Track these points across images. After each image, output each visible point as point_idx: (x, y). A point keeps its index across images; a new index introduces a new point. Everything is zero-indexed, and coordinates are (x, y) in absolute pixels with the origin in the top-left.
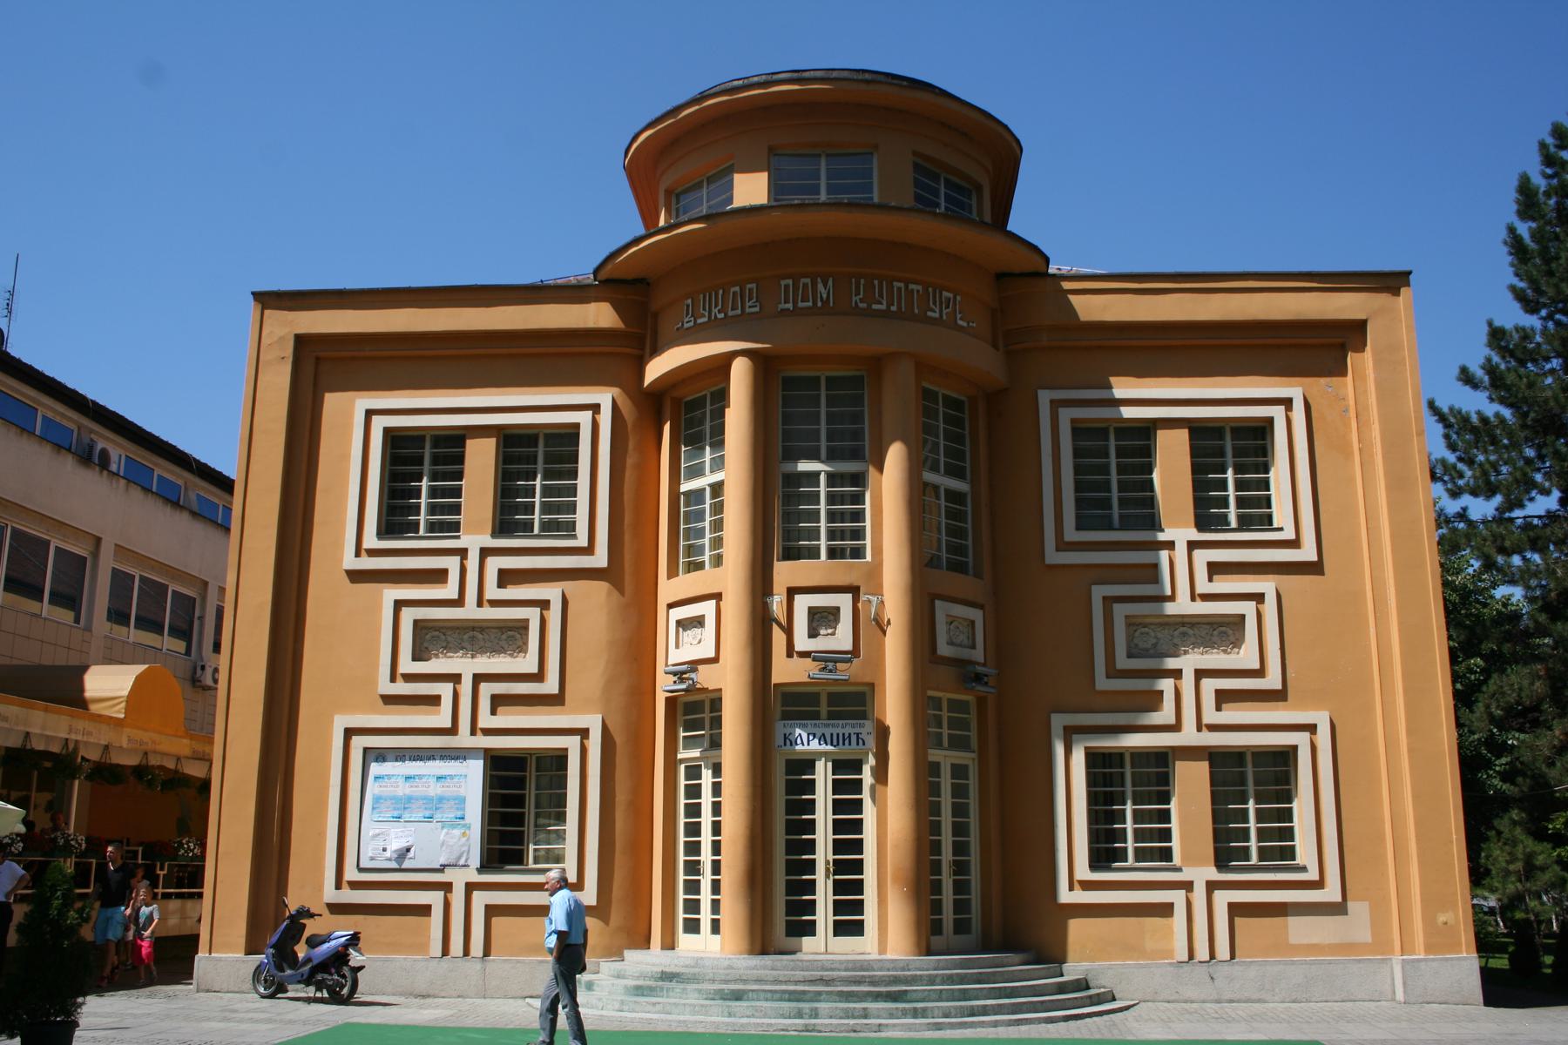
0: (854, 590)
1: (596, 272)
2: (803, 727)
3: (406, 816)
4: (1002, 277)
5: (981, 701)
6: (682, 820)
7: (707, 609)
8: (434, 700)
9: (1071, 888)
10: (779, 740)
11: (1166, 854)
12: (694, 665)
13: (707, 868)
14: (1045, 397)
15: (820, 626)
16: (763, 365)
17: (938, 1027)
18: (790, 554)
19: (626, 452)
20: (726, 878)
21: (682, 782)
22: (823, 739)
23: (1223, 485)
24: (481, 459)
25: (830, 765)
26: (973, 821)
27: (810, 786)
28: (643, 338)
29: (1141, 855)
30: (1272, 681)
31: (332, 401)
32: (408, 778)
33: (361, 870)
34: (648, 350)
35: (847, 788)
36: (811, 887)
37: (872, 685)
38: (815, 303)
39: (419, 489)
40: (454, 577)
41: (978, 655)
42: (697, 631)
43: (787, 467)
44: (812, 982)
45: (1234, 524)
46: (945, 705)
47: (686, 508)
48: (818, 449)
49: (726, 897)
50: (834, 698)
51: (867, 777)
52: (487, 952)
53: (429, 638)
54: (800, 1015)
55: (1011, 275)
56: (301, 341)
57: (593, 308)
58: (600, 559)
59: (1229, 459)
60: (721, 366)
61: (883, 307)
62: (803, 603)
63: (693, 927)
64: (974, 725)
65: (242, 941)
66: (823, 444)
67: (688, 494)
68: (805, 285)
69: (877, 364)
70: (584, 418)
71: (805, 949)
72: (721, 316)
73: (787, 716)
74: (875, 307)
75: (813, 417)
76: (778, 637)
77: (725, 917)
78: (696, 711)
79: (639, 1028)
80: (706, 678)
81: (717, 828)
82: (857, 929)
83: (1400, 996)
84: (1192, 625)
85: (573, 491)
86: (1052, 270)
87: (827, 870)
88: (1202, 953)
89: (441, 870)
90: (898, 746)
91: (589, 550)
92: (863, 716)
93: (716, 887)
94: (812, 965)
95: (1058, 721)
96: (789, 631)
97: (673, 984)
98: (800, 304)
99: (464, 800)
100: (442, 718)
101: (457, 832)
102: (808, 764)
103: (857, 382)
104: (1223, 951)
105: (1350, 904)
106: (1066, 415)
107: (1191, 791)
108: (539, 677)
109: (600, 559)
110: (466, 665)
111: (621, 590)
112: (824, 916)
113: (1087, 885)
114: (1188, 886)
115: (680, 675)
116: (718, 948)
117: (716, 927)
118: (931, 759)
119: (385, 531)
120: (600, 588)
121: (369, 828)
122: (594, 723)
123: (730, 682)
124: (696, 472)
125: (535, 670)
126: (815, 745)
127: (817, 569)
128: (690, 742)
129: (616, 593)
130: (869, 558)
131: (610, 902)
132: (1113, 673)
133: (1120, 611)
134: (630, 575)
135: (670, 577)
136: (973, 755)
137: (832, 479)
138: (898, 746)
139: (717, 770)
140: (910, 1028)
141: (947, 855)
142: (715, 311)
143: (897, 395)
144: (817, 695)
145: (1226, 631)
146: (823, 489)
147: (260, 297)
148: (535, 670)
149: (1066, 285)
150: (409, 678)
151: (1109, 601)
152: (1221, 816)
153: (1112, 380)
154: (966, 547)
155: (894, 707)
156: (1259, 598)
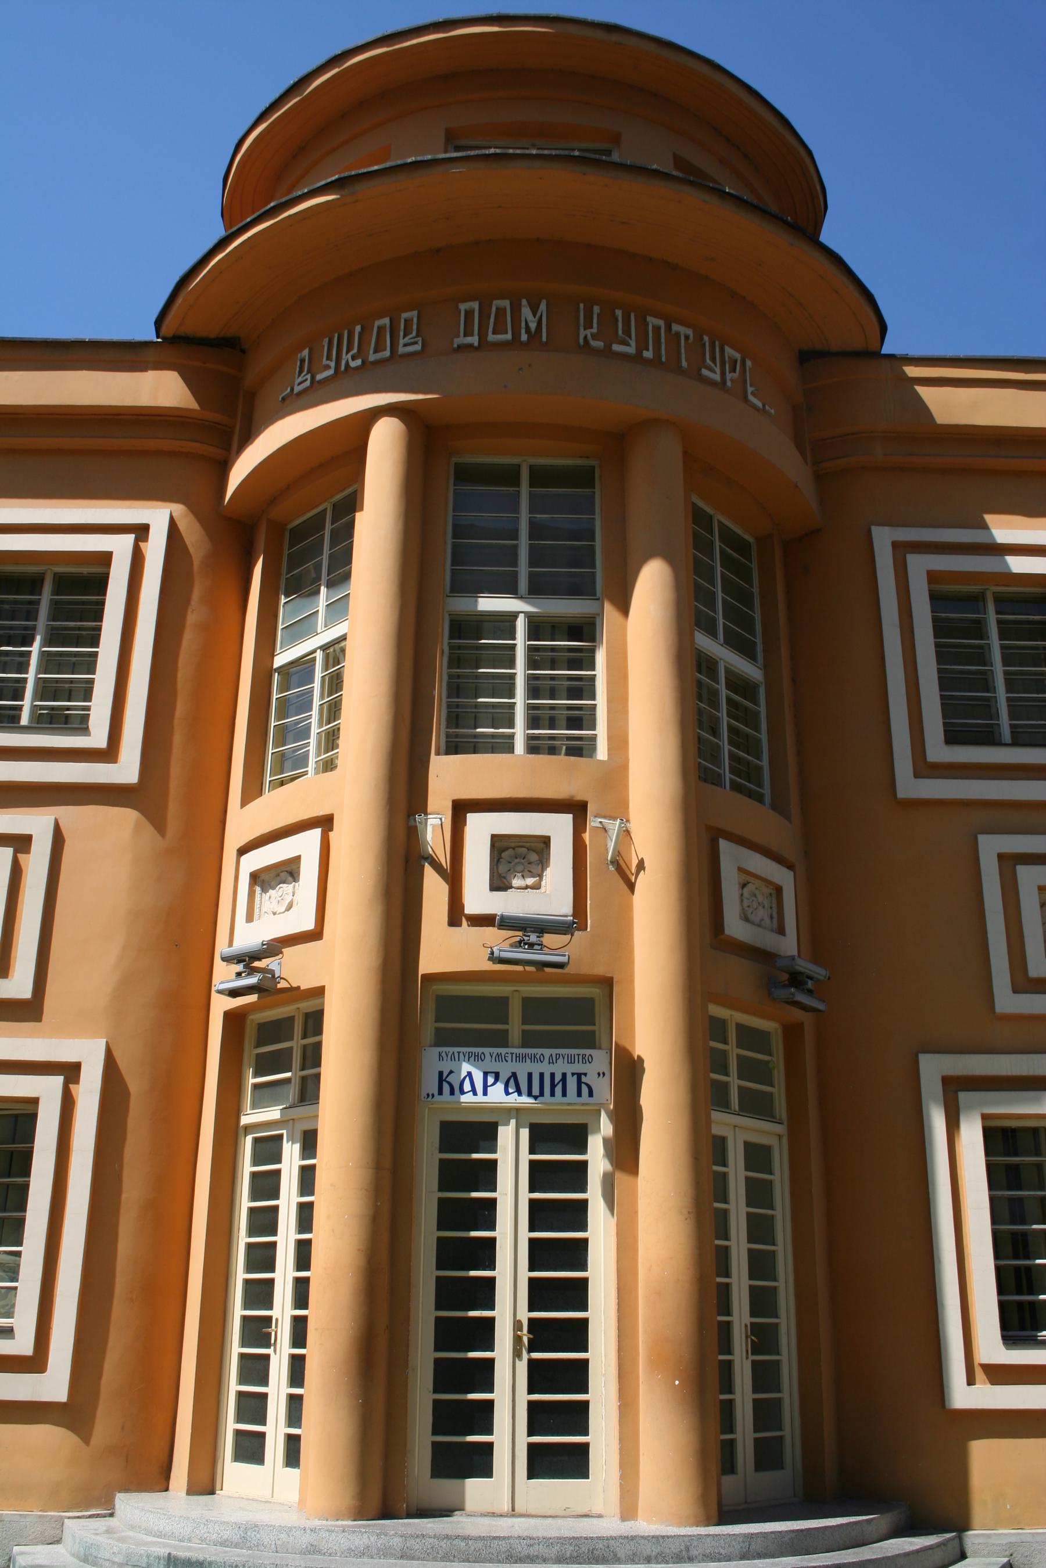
0: (577, 809)
1: (159, 323)
2: (476, 1059)
4: (808, 358)
5: (792, 1033)
6: (242, 1239)
7: (306, 846)
9: (971, 1381)
12: (274, 947)
13: (283, 1332)
14: (883, 538)
15: (512, 871)
16: (429, 440)
19: (188, 601)
20: (314, 1352)
21: (247, 1168)
22: (513, 1083)
25: (525, 1133)
27: (487, 1174)
28: (231, 417)
35: (557, 1181)
36: (483, 1374)
37: (607, 983)
38: (516, 334)
41: (788, 945)
42: (286, 889)
43: (460, 605)
46: (732, 1035)
47: (281, 692)
49: (312, 1391)
51: (596, 1158)
57: (150, 377)
58: (126, 770)
60: (348, 444)
61: (631, 350)
62: (481, 829)
63: (251, 1449)
64: (779, 1075)
67: (283, 670)
68: (501, 311)
69: (618, 443)
70: (121, 546)
71: (470, 1505)
72: (358, 362)
73: (443, 1039)
74: (617, 348)
75: (512, 527)
76: (434, 889)
77: (312, 1432)
78: (278, 1035)
80: (294, 969)
81: (303, 1255)
82: (571, 1462)
85: (90, 663)
87: (517, 1340)
90: (660, 1098)
91: (109, 754)
92: (589, 1041)
93: (297, 1369)
96: (454, 877)
98: (491, 337)
102: (483, 1132)
103: (583, 478)
106: (919, 565)
109: (126, 770)
111: (160, 827)
112: (509, 1435)
113: (1000, 1375)
115: (247, 960)
116: (294, 1497)
117: (293, 1454)
118: (716, 1130)
120: (124, 819)
123: (341, 977)
124: (303, 628)
126: (497, 1094)
128: (265, 1094)
129: (149, 829)
130: (602, 752)
131: (96, 1394)
134: (177, 805)
135: (244, 804)
136: (781, 1129)
137: (536, 628)
138: (660, 1098)
139: (309, 1143)
141: (741, 1316)
142: (346, 357)
143: (655, 486)
144: (503, 1002)
146: (521, 641)
149: (912, 371)
151: (1009, 862)
153: (989, 518)
154: (760, 769)
155: (651, 1021)
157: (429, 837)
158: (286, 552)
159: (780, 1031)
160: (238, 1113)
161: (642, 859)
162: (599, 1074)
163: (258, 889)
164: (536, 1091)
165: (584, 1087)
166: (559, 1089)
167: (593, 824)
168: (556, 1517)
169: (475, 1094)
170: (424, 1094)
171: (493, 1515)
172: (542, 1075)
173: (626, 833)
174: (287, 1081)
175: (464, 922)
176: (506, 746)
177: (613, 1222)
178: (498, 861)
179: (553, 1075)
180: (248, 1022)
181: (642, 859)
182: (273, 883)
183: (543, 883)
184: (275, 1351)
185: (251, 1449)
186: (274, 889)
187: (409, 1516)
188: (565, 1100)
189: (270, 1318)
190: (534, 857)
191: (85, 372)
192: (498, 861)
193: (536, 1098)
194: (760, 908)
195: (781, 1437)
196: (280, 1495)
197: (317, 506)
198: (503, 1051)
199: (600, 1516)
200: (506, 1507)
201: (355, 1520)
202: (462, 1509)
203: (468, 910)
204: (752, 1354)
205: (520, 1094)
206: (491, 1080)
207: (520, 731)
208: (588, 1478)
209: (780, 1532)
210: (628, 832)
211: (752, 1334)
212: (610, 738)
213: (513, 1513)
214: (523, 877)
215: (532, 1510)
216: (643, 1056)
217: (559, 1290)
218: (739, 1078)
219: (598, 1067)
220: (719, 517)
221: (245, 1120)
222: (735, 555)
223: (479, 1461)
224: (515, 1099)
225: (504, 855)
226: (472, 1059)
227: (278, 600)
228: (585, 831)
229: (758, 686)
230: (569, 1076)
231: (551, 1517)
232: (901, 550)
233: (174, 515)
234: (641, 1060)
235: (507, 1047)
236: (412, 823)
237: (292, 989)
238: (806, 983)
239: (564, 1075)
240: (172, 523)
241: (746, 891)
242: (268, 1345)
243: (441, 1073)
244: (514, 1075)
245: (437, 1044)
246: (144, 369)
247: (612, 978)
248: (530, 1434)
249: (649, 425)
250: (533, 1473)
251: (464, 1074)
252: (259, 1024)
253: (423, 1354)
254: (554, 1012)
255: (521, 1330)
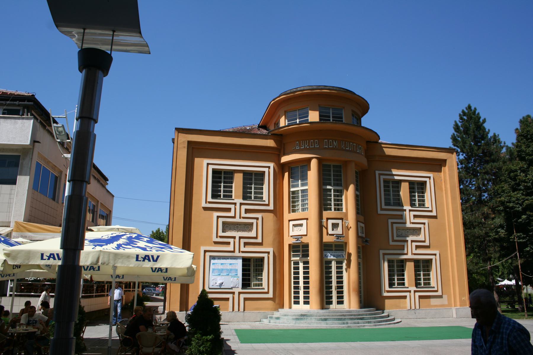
0: (342, 219)
3: (222, 274)
4: (368, 142)
7: (304, 222)
8: (229, 243)
11: (403, 284)
14: (377, 172)
16: (320, 161)
17: (376, 325)
18: (326, 209)
22: (334, 256)
23: (251, 188)
24: (238, 179)
27: (331, 268)
29: (398, 284)
30: (259, 240)
31: (197, 160)
32: (222, 264)
33: (210, 289)
34: (282, 153)
35: (339, 268)
37: (346, 243)
39: (221, 186)
40: (233, 210)
43: (324, 187)
44: (341, 316)
45: (417, 206)
50: (336, 246)
52: (244, 310)
53: (227, 226)
54: (344, 324)
55: (370, 142)
56: (189, 143)
58: (271, 207)
59: (416, 190)
60: (310, 160)
63: (297, 303)
65: (179, 308)
66: (332, 182)
67: (292, 192)
69: (346, 163)
75: (332, 177)
79: (305, 328)
80: (304, 240)
83: (455, 316)
84: (248, 225)
86: (380, 141)
88: (413, 307)
89: (231, 289)
90: (354, 258)
92: (342, 250)
94: (334, 312)
95: (382, 252)
96: (327, 228)
97: (305, 317)
99: (237, 270)
100: (231, 248)
101: (236, 278)
102: (330, 262)
104: (417, 307)
105: (443, 296)
106: (382, 177)
107: (410, 268)
108: (256, 238)
110: (238, 234)
112: (334, 299)
113: (388, 292)
114: (410, 291)
119: (213, 196)
120: (271, 215)
121: (212, 278)
122: (271, 250)
125: (255, 236)
126: (332, 257)
128: (294, 256)
130: (344, 210)
132: (394, 241)
133: (395, 226)
138: (354, 258)
139: (306, 263)
140: (370, 326)
142: (306, 146)
143: (351, 172)
145: (417, 231)
147: (176, 129)
148: (255, 236)
149: (383, 146)
150: (221, 237)
151: (392, 223)
152: (417, 275)
153: (392, 170)
156: (424, 224)
176: (330, 209)
207: (333, 207)
217: (340, 282)
232: (380, 175)
249: (350, 161)
254: (339, 247)
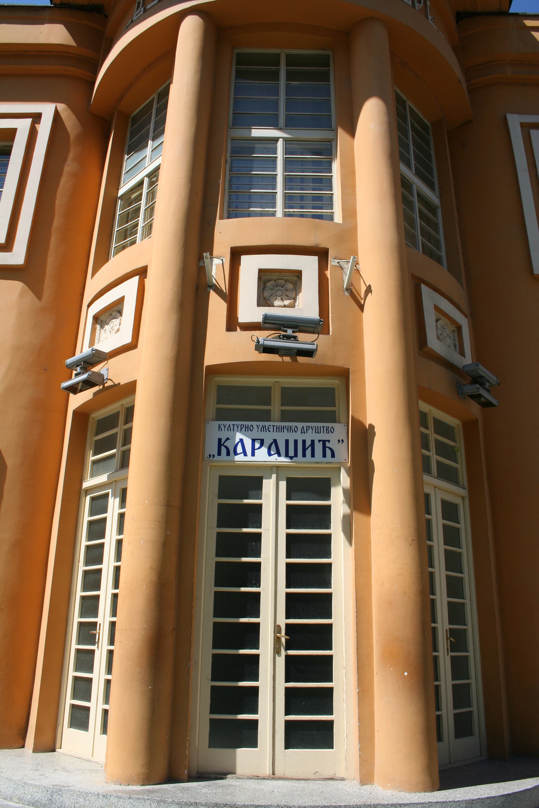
0: (322, 255)
5: (469, 427)
10: (212, 447)
13: (104, 633)
14: (515, 122)
19: (65, 159)
22: (274, 447)
25: (283, 485)
26: (468, 575)
27: (254, 514)
36: (251, 668)
37: (344, 375)
43: (240, 133)
46: (431, 424)
48: (277, 116)
50: (290, 396)
51: (338, 503)
62: (250, 266)
63: (80, 719)
64: (461, 455)
73: (221, 415)
76: (217, 307)
80: (114, 372)
82: (319, 736)
87: (277, 640)
90: (388, 456)
96: (231, 298)
102: (253, 484)
111: (38, 294)
112: (270, 713)
123: (144, 371)
126: (262, 455)
127: (273, 224)
129: (30, 295)
141: (443, 624)
143: (370, 54)
149: (529, 23)
157: (214, 273)
158: (129, 130)
159: (461, 426)
160: (81, 480)
161: (370, 285)
162: (339, 441)
163: (98, 327)
164: (291, 453)
165: (327, 450)
166: (309, 452)
167: (332, 263)
168: (308, 779)
169: (245, 455)
170: (207, 455)
171: (258, 778)
172: (296, 442)
173: (356, 271)
174: (112, 456)
175: (238, 328)
177: (351, 550)
178: (264, 289)
179: (304, 442)
180: (91, 419)
181: (370, 285)
182: (108, 320)
183: (297, 304)
184: (98, 647)
185: (80, 719)
186: (107, 324)
187: (191, 779)
188: (313, 460)
189: (96, 623)
190: (290, 286)
191: (4, 25)
192: (264, 289)
193: (291, 458)
194: (448, 338)
195: (471, 713)
196: (94, 755)
197: (148, 98)
198: (267, 424)
199: (343, 779)
200: (268, 771)
201: (143, 785)
202: (234, 773)
203: (241, 320)
204: (451, 652)
205: (279, 455)
206: (257, 445)
208: (332, 748)
209: (494, 797)
210: (358, 271)
211: (450, 637)
212: (343, 210)
213: (273, 776)
214: (282, 299)
215: (288, 775)
216: (373, 424)
217: (309, 602)
218: (437, 454)
219: (339, 436)
220: (409, 103)
221: (85, 485)
222: (419, 128)
223: (248, 735)
224: (275, 459)
225: (268, 285)
226: (243, 430)
227: (123, 158)
228: (327, 270)
229: (437, 208)
230: (316, 443)
231: (303, 779)
233: (59, 109)
234: (372, 427)
235: (269, 420)
236: (201, 264)
237: (115, 386)
238: (485, 384)
239: (313, 442)
240: (57, 114)
241: (439, 323)
242: (94, 643)
243: (220, 440)
244: (275, 441)
245: (218, 419)
246: (43, 23)
247: (348, 370)
248: (287, 714)
250: (288, 746)
251: (237, 440)
252: (98, 421)
253: (203, 651)
255: (280, 632)
